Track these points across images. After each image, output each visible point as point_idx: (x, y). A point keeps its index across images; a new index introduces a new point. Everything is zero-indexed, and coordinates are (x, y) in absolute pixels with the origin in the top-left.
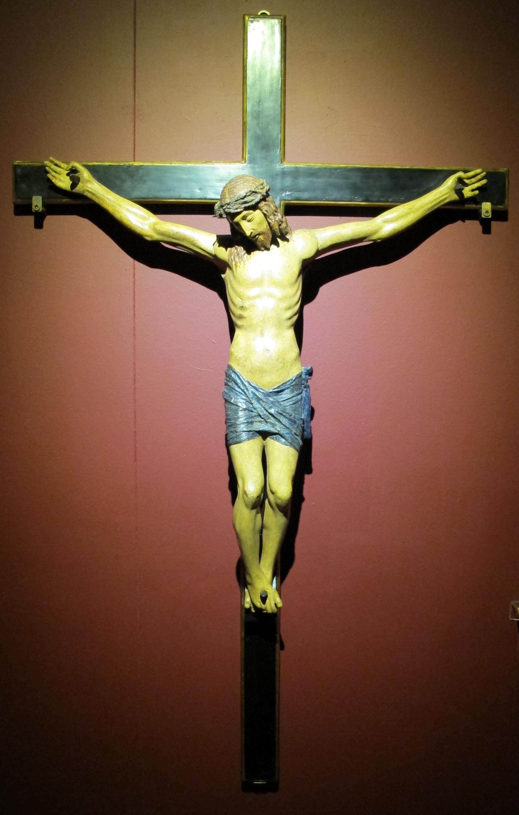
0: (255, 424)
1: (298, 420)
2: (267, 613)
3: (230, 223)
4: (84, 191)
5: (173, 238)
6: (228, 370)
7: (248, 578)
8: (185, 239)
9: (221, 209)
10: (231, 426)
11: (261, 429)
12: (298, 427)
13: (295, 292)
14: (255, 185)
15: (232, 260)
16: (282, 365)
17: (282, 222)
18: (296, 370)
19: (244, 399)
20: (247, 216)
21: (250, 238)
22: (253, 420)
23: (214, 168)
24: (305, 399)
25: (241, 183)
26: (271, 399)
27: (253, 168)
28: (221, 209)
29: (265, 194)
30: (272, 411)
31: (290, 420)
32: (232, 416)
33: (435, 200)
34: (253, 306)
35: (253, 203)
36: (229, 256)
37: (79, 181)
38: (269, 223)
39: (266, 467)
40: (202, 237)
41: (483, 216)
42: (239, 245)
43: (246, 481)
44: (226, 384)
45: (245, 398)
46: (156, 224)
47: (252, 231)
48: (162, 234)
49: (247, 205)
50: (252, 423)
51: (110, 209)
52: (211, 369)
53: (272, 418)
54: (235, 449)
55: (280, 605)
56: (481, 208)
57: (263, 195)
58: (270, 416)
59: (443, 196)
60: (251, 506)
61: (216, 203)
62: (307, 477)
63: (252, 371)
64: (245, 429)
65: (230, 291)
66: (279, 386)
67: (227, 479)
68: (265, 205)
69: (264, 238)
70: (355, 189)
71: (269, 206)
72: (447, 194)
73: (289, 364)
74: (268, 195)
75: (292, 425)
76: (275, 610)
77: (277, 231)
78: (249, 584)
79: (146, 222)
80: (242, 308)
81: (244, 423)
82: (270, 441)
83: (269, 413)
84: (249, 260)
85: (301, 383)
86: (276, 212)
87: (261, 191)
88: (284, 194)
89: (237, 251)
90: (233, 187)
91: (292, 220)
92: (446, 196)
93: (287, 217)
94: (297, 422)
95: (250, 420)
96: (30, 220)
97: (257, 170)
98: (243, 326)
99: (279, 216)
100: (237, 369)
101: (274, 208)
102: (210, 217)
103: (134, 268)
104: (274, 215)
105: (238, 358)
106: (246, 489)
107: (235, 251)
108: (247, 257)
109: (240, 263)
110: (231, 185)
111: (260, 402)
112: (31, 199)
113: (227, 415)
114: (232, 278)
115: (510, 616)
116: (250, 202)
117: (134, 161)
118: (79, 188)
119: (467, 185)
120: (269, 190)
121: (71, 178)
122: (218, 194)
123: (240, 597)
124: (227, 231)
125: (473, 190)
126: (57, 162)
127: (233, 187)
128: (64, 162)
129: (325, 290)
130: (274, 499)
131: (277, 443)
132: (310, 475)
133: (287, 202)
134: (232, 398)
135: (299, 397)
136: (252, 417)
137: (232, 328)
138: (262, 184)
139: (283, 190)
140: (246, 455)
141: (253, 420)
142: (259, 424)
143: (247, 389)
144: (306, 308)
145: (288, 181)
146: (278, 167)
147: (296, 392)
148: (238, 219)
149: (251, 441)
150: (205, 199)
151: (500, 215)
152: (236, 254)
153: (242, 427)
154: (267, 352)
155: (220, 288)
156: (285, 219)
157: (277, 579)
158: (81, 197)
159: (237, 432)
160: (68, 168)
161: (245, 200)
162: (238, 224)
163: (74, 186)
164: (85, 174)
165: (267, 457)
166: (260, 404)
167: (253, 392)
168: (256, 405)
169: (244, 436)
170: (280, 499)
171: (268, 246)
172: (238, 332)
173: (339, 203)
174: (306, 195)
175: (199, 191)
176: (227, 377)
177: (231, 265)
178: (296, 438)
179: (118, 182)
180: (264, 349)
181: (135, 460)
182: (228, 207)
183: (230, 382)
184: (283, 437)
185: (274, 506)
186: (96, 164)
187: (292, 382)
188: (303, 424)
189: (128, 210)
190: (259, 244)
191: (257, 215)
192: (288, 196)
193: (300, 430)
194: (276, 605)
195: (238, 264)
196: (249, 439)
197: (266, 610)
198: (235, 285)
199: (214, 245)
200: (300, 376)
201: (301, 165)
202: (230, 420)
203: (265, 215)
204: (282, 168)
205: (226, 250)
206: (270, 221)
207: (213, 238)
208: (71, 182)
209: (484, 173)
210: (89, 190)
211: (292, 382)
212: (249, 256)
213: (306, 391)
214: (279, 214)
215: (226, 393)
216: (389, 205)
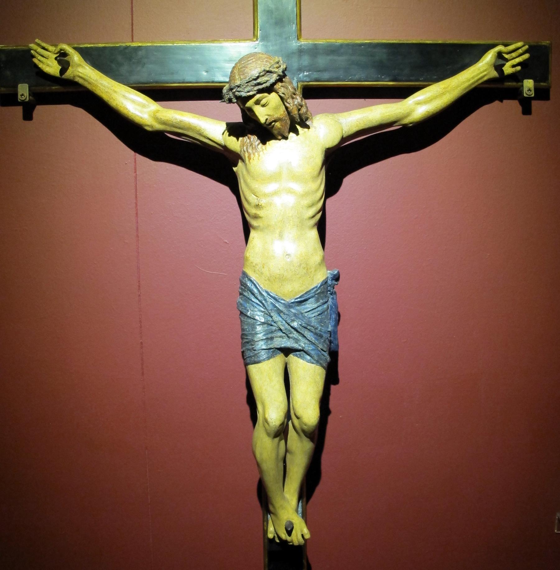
0: (275, 339)
1: (325, 333)
2: (293, 545)
3: (241, 109)
4: (74, 77)
5: (176, 127)
6: (243, 278)
7: (271, 508)
8: (190, 128)
9: (231, 93)
10: (248, 342)
11: (282, 346)
12: (325, 341)
13: (318, 186)
14: (270, 63)
15: (244, 151)
16: (305, 271)
17: (302, 106)
18: (321, 276)
19: (262, 312)
21: (265, 126)
22: (273, 335)
23: (222, 47)
24: (332, 307)
25: (253, 62)
26: (293, 311)
27: (266, 46)
28: (231, 93)
29: (281, 74)
30: (295, 324)
31: (316, 334)
32: (249, 331)
33: (473, 78)
34: (271, 204)
35: (268, 84)
36: (240, 147)
37: (69, 66)
38: (287, 108)
39: (288, 390)
40: (209, 125)
41: (525, 95)
42: (252, 134)
43: (267, 407)
44: (241, 294)
45: (263, 310)
46: (158, 111)
47: (267, 117)
48: (164, 123)
49: (260, 87)
50: (272, 339)
51: (105, 97)
52: (224, 272)
53: (295, 332)
54: (253, 369)
55: (307, 536)
56: (523, 86)
57: (279, 75)
58: (293, 330)
59: (481, 73)
60: (273, 434)
61: (224, 86)
62: (333, 387)
63: (271, 279)
64: (264, 347)
65: (242, 186)
66: (302, 295)
67: (245, 392)
68: (282, 86)
69: (281, 125)
70: (381, 68)
71: (287, 88)
72: (485, 70)
73: (313, 270)
74: (285, 76)
75: (317, 340)
76: (302, 541)
77: (297, 117)
78: (273, 513)
79: (145, 110)
80: (257, 206)
81: (262, 340)
82: (293, 359)
83: (292, 327)
84: (265, 151)
85: (326, 290)
86: (295, 94)
87: (276, 70)
88: (301, 75)
89: (250, 141)
90: (244, 67)
91: (312, 103)
92: (485, 73)
93: (308, 101)
95: (269, 336)
96: (19, 110)
97: (271, 48)
98: (259, 226)
99: (298, 99)
100: (253, 277)
101: (292, 90)
102: (217, 102)
103: (135, 162)
104: (293, 98)
105: (254, 264)
106: (267, 416)
107: (248, 141)
108: (262, 147)
109: (254, 154)
110: (241, 64)
111: (281, 314)
112: (16, 87)
113: (243, 330)
114: (245, 172)
115: (556, 527)
116: (264, 83)
117: (133, 41)
118: (69, 74)
119: (507, 60)
120: (286, 69)
121: (60, 62)
122: (226, 76)
123: (262, 521)
124: (238, 118)
125: (514, 66)
126: (44, 44)
127: (244, 67)
128: (52, 45)
129: (349, 181)
130: (300, 425)
131: (301, 361)
132: (337, 385)
133: (306, 83)
134: (248, 311)
135: (325, 306)
136: (272, 332)
137: (247, 229)
138: (278, 63)
139: (300, 70)
140: (266, 377)
141: (273, 335)
142: (280, 339)
143: (265, 300)
144: (328, 201)
145: (306, 60)
146: (294, 44)
147: (321, 301)
148: (250, 103)
149: (271, 360)
150: (213, 82)
151: (542, 94)
152: (249, 145)
153: (261, 345)
154: (287, 257)
155: (232, 183)
156: (305, 102)
157: (302, 503)
158: (72, 83)
159: (255, 350)
160: (56, 52)
161: (259, 81)
162: (250, 110)
163: (63, 71)
164: (76, 57)
165: (290, 376)
166: (281, 317)
167: (272, 303)
168: (276, 317)
169: (263, 355)
170: (306, 425)
171: (286, 134)
172: (253, 234)
173: (363, 83)
174: (326, 75)
175: (206, 74)
176: (242, 285)
177: (243, 157)
178: (323, 355)
179: (113, 66)
180: (284, 254)
181: (143, 374)
182: (239, 89)
183: (245, 291)
184: (309, 355)
185: (300, 431)
186: (89, 46)
187: (317, 290)
188: (330, 336)
189: (124, 96)
190: (275, 132)
191: (273, 98)
192: (305, 77)
193: (327, 344)
194: (303, 536)
195: (252, 156)
196: (269, 358)
197: (292, 541)
198: (249, 180)
199: (223, 134)
200: (325, 282)
201: (320, 42)
202: (246, 335)
203: (282, 98)
204: (299, 46)
205: (238, 139)
206: (288, 105)
207: (223, 126)
208: (60, 67)
209: (527, 47)
210: (80, 75)
211: (317, 290)
212: (264, 147)
213: (333, 298)
214: (298, 97)
215: (241, 304)
216: (420, 85)
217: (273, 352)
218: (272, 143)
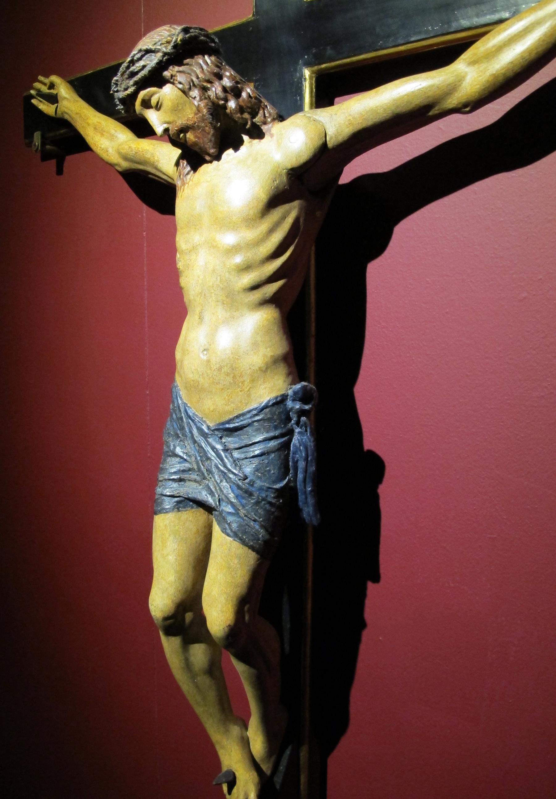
12: (257, 503)
16: (229, 379)
20: (150, 100)
47: (166, 126)
69: (196, 137)
73: (247, 379)
94: (256, 494)
140: (169, 539)
169: (168, 504)
191: (168, 92)
217: (178, 502)
218: (205, 168)
